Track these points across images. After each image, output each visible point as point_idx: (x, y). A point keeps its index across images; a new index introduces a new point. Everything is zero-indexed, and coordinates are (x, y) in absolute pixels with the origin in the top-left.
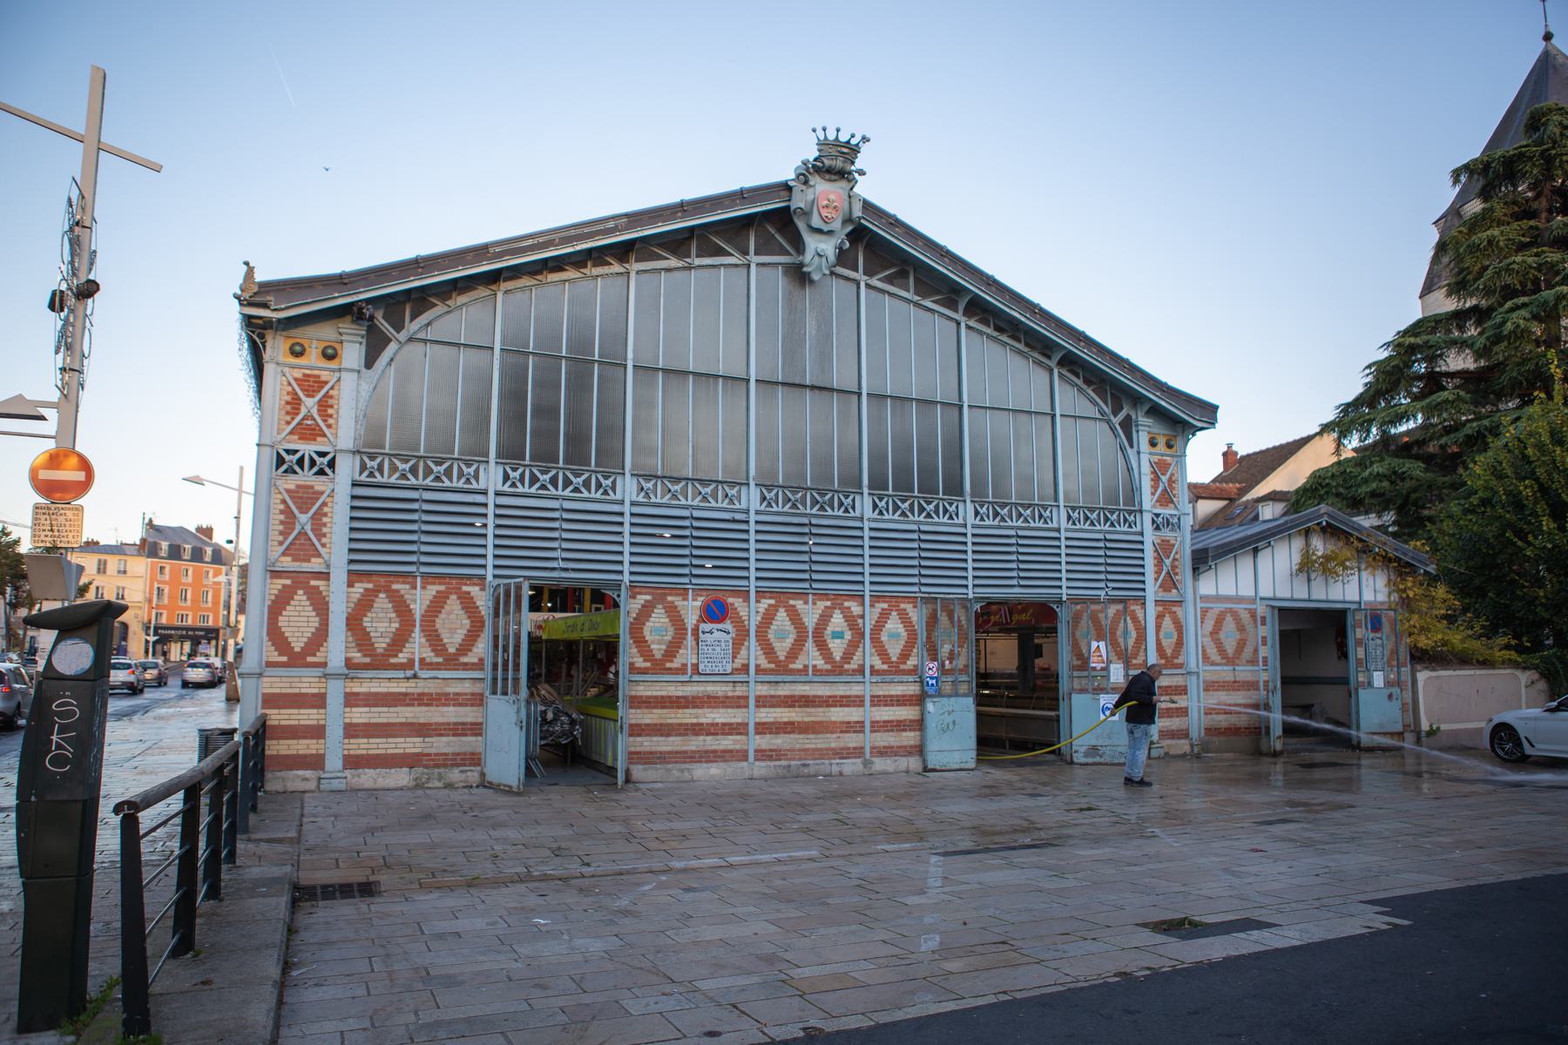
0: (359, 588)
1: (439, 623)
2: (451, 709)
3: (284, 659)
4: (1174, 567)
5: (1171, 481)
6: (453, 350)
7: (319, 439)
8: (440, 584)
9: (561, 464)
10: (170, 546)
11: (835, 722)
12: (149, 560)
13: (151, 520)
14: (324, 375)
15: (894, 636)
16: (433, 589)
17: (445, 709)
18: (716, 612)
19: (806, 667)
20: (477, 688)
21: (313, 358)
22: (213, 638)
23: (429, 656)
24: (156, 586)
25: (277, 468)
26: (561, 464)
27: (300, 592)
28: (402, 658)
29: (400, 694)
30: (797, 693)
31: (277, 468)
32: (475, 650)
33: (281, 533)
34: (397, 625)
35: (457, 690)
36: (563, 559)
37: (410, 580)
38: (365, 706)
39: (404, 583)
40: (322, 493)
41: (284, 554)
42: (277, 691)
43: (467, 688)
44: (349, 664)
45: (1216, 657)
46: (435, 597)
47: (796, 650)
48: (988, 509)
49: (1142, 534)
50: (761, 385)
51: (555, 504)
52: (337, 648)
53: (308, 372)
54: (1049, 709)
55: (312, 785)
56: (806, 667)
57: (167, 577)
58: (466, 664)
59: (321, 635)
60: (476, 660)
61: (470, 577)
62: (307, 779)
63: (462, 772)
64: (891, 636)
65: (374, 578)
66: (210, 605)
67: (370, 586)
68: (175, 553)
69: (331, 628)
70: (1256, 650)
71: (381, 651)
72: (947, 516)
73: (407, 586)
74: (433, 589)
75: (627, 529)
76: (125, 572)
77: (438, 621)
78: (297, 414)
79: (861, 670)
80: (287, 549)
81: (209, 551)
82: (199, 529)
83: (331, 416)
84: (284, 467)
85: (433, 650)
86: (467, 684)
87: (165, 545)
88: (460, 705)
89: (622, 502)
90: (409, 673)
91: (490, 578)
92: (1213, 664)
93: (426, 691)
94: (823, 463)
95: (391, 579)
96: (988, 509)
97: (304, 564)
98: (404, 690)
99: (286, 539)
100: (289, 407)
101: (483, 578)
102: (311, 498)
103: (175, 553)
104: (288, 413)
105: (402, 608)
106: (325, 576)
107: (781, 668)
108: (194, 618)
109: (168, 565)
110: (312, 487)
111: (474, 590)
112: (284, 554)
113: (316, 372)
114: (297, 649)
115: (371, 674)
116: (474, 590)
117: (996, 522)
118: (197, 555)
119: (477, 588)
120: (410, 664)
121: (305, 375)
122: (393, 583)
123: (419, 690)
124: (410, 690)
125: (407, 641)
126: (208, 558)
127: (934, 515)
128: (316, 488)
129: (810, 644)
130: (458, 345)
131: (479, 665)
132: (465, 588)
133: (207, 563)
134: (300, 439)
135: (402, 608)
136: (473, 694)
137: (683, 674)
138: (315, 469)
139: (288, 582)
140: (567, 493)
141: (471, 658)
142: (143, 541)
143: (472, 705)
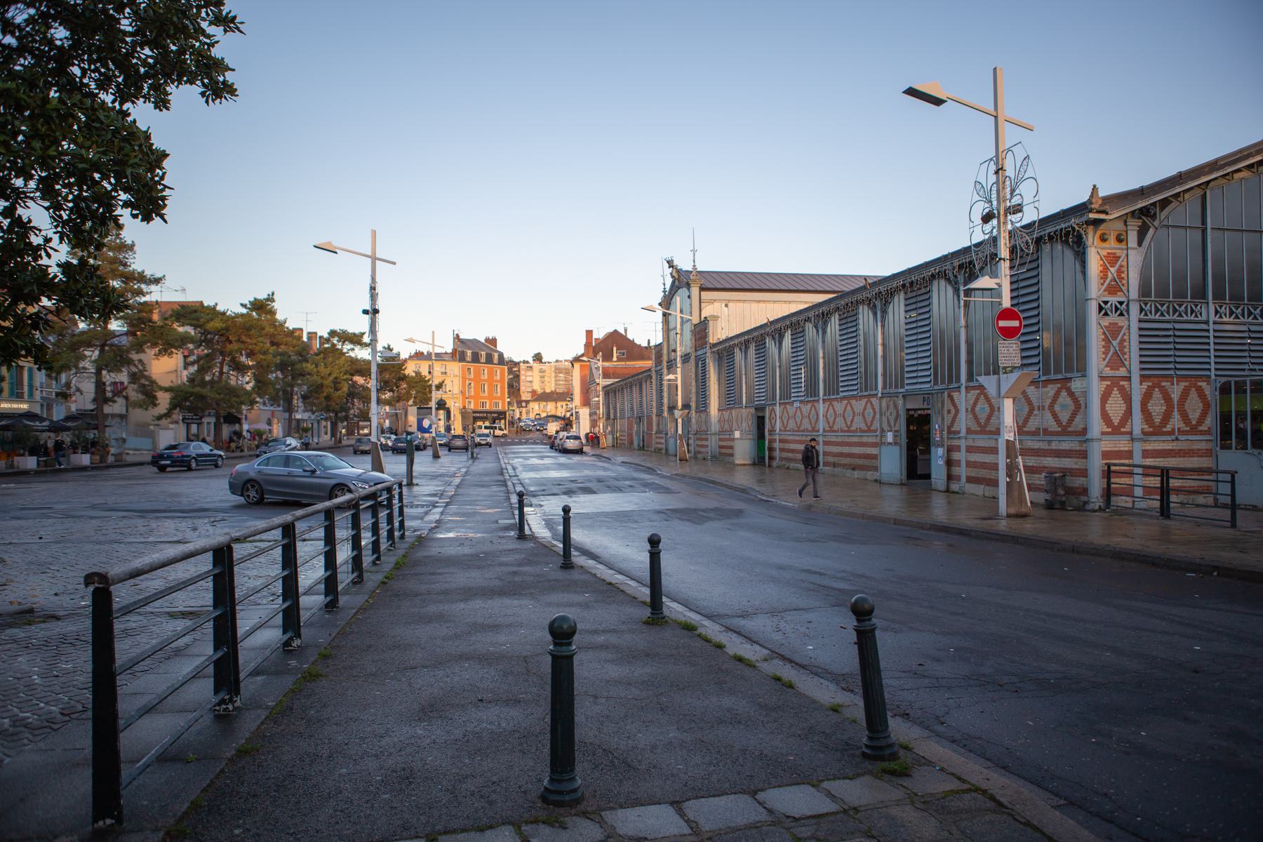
0: (1145, 385)
1: (1187, 406)
2: (1196, 459)
3: (1110, 430)
5: (1119, 272)
6: (1182, 231)
7: (1119, 293)
8: (1186, 381)
9: (1246, 302)
10: (473, 353)
12: (461, 364)
13: (458, 335)
14: (1118, 253)
15: (1063, 406)
16: (1183, 384)
17: (1193, 459)
20: (1209, 446)
21: (1112, 242)
22: (502, 419)
23: (1182, 425)
24: (467, 382)
25: (1099, 313)
26: (1246, 302)
27: (1115, 389)
28: (1168, 428)
29: (1169, 450)
31: (1099, 313)
32: (1206, 422)
33: (1104, 353)
34: (1165, 408)
35: (1199, 447)
36: (1252, 363)
37: (1170, 379)
38: (1152, 457)
39: (1167, 381)
40: (1122, 327)
41: (1107, 366)
42: (1108, 449)
43: (1203, 446)
44: (1144, 433)
46: (1184, 390)
47: (1167, 417)
48: (1151, 306)
50: (1215, 231)
51: (1169, 326)
52: (1137, 423)
53: (1110, 251)
54: (1127, 459)
55: (1130, 505)
56: (1173, 430)
57: (472, 376)
58: (1201, 431)
59: (1128, 413)
60: (1206, 429)
61: (1201, 376)
62: (1127, 502)
63: (1204, 497)
64: (1063, 406)
65: (1152, 379)
66: (499, 394)
67: (1150, 384)
68: (476, 358)
69: (1133, 410)
71: (1158, 424)
72: (1194, 315)
73: (1169, 384)
74: (1183, 384)
75: (1212, 340)
76: (446, 373)
78: (1106, 278)
80: (1108, 363)
81: (496, 356)
82: (487, 340)
83: (1123, 278)
84: (1103, 312)
85: (1184, 423)
86: (1204, 444)
87: (469, 353)
88: (1200, 456)
89: (1207, 322)
90: (1174, 437)
91: (1213, 377)
93: (1183, 448)
94: (1180, 279)
95: (1161, 379)
96: (1151, 306)
97: (1117, 372)
98: (1170, 448)
99: (1106, 357)
100: (1102, 274)
101: (1209, 377)
103: (476, 358)
104: (1102, 278)
105: (1167, 397)
106: (1129, 379)
107: (1155, 430)
108: (490, 405)
109: (473, 366)
110: (1117, 324)
111: (1203, 384)
112: (1107, 366)
113: (1114, 251)
114: (1116, 424)
115: (1154, 438)
116: (1203, 384)
117: (1250, 320)
118: (489, 360)
119: (1205, 383)
120: (1171, 433)
121: (1108, 253)
123: (1178, 448)
124: (1174, 448)
125: (1170, 418)
126: (496, 361)
127: (1184, 315)
128: (1120, 324)
129: (1176, 414)
130: (1224, 230)
131: (1208, 432)
132: (1199, 384)
133: (468, 362)
134: (1109, 294)
135: (1167, 397)
136: (1207, 450)
138: (1119, 312)
139: (1109, 383)
140: (1250, 320)
141: (1203, 428)
142: (455, 351)
143: (1206, 456)
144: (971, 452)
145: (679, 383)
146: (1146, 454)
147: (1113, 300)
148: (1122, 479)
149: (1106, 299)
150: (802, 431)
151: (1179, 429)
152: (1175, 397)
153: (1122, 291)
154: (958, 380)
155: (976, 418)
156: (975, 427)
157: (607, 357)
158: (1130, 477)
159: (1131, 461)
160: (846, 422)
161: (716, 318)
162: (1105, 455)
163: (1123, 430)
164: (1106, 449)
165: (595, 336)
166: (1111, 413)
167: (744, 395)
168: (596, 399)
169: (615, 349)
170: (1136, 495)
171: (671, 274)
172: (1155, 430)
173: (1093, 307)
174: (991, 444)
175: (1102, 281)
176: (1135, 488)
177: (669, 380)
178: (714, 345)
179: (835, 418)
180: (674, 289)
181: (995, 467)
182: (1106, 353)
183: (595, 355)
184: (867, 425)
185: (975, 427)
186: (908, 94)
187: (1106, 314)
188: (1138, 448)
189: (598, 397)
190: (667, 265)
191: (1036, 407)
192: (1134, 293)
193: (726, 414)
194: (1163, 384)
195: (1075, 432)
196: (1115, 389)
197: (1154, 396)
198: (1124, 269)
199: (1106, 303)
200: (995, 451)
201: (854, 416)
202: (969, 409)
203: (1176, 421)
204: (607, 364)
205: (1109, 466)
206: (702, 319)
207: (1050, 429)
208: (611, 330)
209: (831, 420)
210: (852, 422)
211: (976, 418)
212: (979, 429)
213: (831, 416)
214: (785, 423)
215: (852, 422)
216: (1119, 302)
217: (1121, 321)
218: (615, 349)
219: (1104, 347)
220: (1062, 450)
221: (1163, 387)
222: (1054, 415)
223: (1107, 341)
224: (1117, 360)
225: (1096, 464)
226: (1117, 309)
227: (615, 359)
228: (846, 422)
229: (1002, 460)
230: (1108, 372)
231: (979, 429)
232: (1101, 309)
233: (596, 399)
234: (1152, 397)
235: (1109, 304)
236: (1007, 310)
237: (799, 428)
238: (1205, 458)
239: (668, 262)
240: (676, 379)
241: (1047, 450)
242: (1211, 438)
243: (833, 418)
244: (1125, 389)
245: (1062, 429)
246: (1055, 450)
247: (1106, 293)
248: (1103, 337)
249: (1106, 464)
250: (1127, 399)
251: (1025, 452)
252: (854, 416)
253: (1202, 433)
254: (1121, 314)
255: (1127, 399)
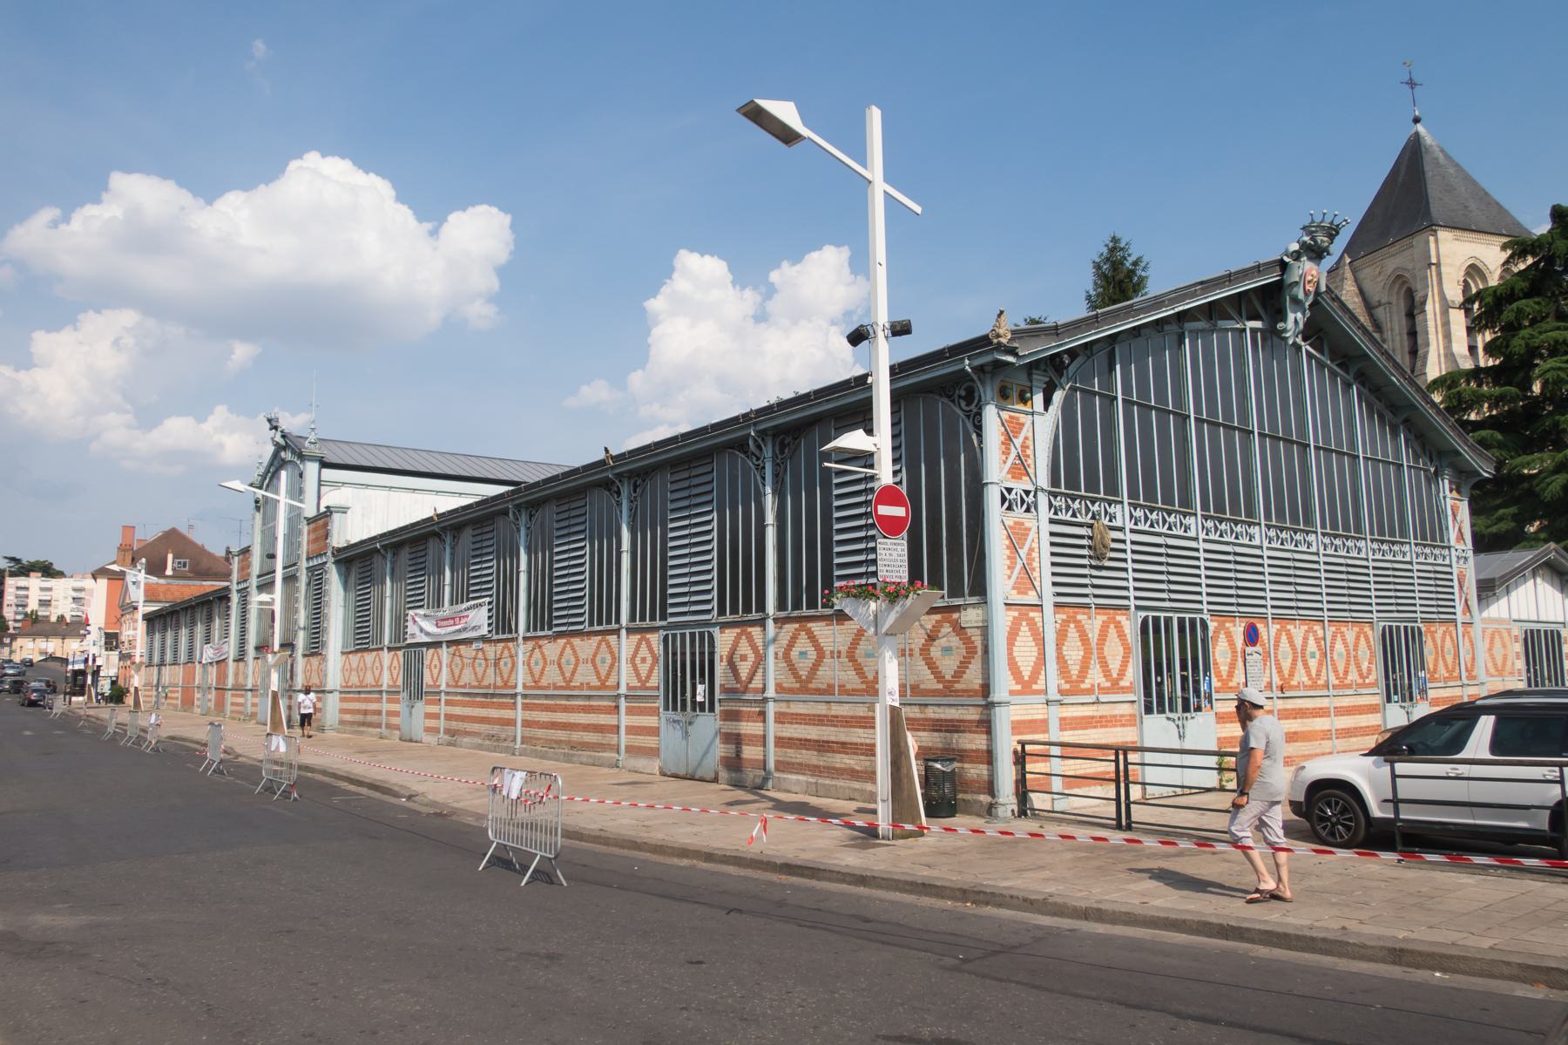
4: (1030, 560)
11: (1316, 731)
18: (1252, 636)
19: (1093, 686)
23: (1305, 679)
30: (1297, 706)
37: (1086, 610)
38: (1071, 729)
39: (1084, 614)
40: (1030, 529)
45: (1492, 671)
49: (1450, 566)
52: (1052, 680)
56: (1093, 686)
60: (1128, 684)
65: (1066, 609)
67: (1064, 617)
70: (1513, 664)
72: (1167, 526)
73: (1085, 617)
77: (1106, 648)
78: (1009, 454)
79: (1326, 686)
83: (1028, 456)
84: (1006, 504)
92: (1493, 676)
93: (1104, 714)
95: (1076, 610)
99: (1012, 573)
101: (1454, 621)
102: (1022, 534)
106: (1039, 607)
107: (1073, 687)
110: (1022, 524)
121: (1010, 417)
122: (1076, 613)
123: (1099, 714)
124: (1095, 714)
134: (1013, 477)
136: (1130, 716)
137: (831, 694)
144: (783, 723)
145: (277, 608)
146: (1066, 724)
147: (1020, 486)
148: (1102, 769)
149: (1009, 485)
150: (464, 687)
151: (1099, 684)
152: (1093, 636)
153: (1028, 474)
154: (761, 606)
155: (792, 667)
156: (790, 682)
157: (156, 568)
158: (1046, 761)
159: (1046, 735)
160: (563, 673)
161: (344, 510)
162: (1017, 727)
163: (1035, 687)
164: (1019, 718)
165: (139, 535)
166: (1020, 662)
167: (447, 590)
168: (131, 632)
169: (170, 557)
170: (1054, 790)
171: (272, 439)
172: (1073, 687)
173: (992, 497)
174: (861, 711)
175: (1004, 457)
176: (1053, 777)
177: (261, 603)
178: (339, 550)
179: (544, 667)
180: (276, 464)
181: (870, 750)
182: (1011, 568)
183: (134, 561)
184: (599, 677)
185: (790, 682)
186: (745, 115)
187: (1010, 508)
188: (1056, 713)
189: (135, 629)
190: (268, 425)
191: (828, 653)
192: (1043, 481)
193: (355, 659)
194: (1079, 617)
195: (966, 691)
196: (1024, 623)
197: (1069, 635)
198: (1030, 443)
199: (1009, 490)
200: (868, 723)
201: (576, 665)
202: (780, 654)
203: (1095, 676)
204: (154, 579)
205: (1023, 744)
206: (323, 509)
207: (922, 686)
208: (167, 528)
209: (537, 670)
210: (573, 673)
211: (792, 667)
212: (798, 685)
213: (537, 663)
214: (457, 674)
215: (573, 673)
216: (1025, 491)
217: (1029, 521)
218: (170, 557)
219: (1009, 558)
220: (946, 720)
221: (1080, 621)
222: (931, 665)
223: (1014, 548)
224: (1027, 579)
225: (1006, 744)
226: (1023, 501)
227: (169, 572)
228: (563, 673)
229: (881, 738)
230: (1016, 598)
231: (798, 685)
232: (1004, 499)
233: (131, 632)
234: (1066, 636)
235: (1014, 492)
236: (887, 489)
237: (457, 682)
238: (1129, 728)
239: (270, 421)
240: (272, 603)
241: (919, 719)
242: (1135, 698)
243: (539, 667)
244: (1036, 624)
245: (1112, 685)
246: (934, 720)
247: (1010, 476)
248: (1007, 542)
249: (1019, 742)
250: (1040, 641)
251: (916, 725)
252: (576, 665)
253: (1124, 690)
254: (1028, 510)
255: (1040, 641)
